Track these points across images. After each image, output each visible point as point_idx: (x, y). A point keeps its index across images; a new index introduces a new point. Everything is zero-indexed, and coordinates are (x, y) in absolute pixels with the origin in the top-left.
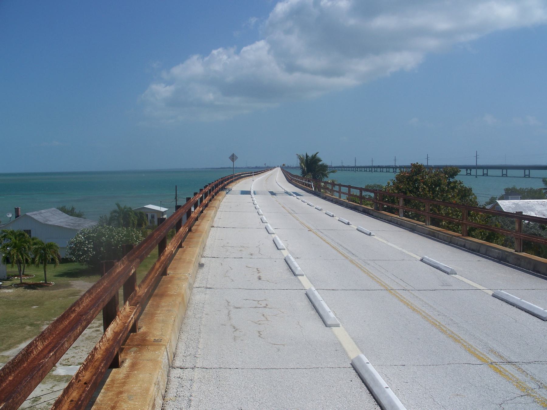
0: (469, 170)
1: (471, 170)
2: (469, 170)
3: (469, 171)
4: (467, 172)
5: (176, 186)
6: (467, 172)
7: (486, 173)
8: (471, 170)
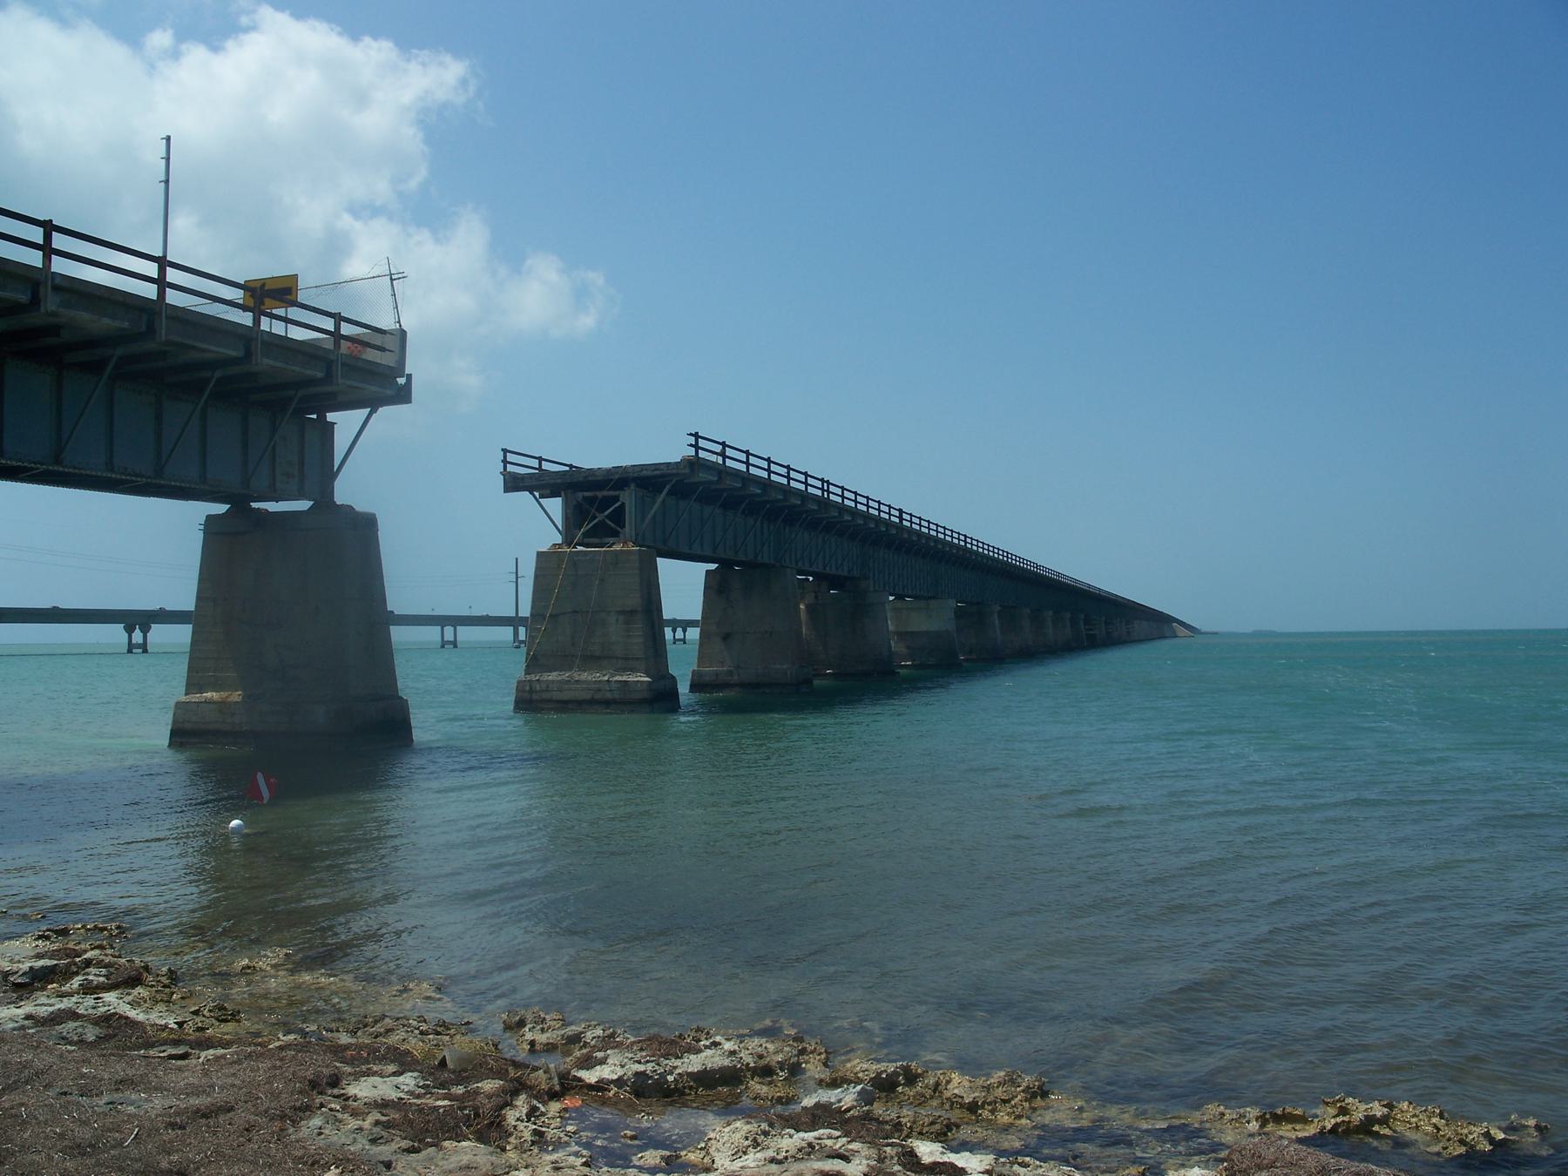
0: (679, 630)
1: (685, 631)
2: (679, 630)
3: (137, 636)
4: (674, 637)
5: (517, 559)
6: (674, 637)
7: (452, 639)
8: (685, 631)
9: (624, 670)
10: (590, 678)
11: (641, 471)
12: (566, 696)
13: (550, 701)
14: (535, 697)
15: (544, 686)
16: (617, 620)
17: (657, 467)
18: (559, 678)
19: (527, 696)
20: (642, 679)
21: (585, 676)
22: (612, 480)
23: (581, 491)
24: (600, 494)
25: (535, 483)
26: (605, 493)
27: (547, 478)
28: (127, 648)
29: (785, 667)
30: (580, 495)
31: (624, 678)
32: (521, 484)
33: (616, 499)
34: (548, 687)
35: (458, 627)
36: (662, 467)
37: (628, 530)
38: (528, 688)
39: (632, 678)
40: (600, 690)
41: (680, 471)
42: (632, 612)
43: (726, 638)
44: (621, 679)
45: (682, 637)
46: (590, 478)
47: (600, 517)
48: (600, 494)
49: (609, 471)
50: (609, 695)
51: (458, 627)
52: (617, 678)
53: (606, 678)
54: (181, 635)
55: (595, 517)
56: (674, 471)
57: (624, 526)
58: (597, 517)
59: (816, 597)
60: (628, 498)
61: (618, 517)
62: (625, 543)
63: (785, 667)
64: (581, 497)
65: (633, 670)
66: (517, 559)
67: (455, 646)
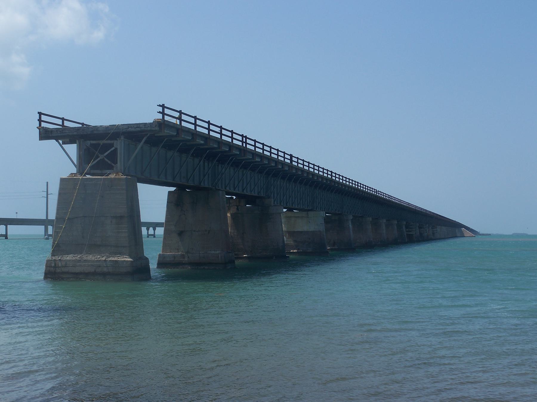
0: (151, 229)
1: (154, 229)
2: (151, 229)
5: (47, 182)
6: (148, 233)
8: (154, 229)
9: (115, 254)
10: (93, 258)
11: (128, 128)
12: (78, 270)
13: (68, 273)
14: (58, 270)
15: (64, 263)
16: (111, 222)
17: (138, 126)
18: (74, 258)
19: (52, 269)
20: (127, 259)
21: (90, 257)
22: (109, 133)
23: (90, 140)
24: (101, 142)
25: (59, 135)
26: (105, 142)
27: (67, 131)
28: (147, 236)
29: (218, 252)
30: (89, 143)
31: (116, 259)
32: (51, 135)
33: (112, 145)
34: (66, 264)
35: (8, 226)
36: (141, 126)
37: (119, 165)
38: (53, 265)
39: (121, 259)
40: (100, 266)
41: (153, 129)
42: (121, 217)
43: (181, 234)
44: (113, 259)
45: (153, 233)
46: (95, 132)
47: (101, 157)
48: (101, 142)
49: (107, 128)
50: (105, 270)
51: (8, 226)
52: (110, 259)
53: (104, 259)
54: (160, 231)
55: (97, 157)
56: (149, 129)
57: (117, 163)
58: (99, 157)
59: (237, 209)
60: (119, 145)
61: (113, 157)
62: (117, 173)
63: (218, 252)
64: (89, 144)
65: (121, 254)
66: (47, 182)
67: (6, 238)
